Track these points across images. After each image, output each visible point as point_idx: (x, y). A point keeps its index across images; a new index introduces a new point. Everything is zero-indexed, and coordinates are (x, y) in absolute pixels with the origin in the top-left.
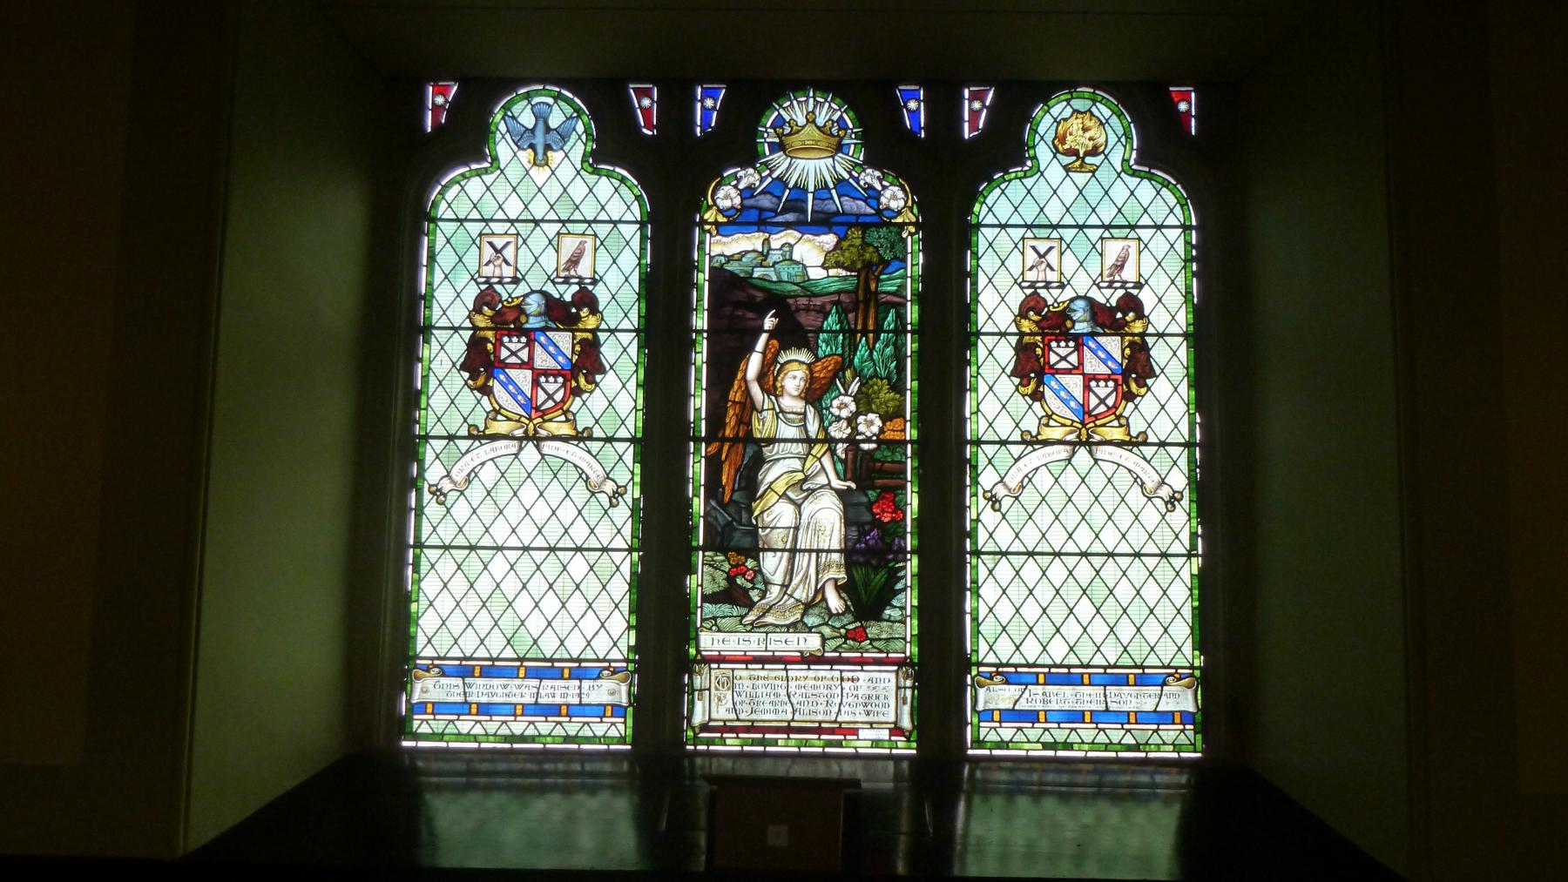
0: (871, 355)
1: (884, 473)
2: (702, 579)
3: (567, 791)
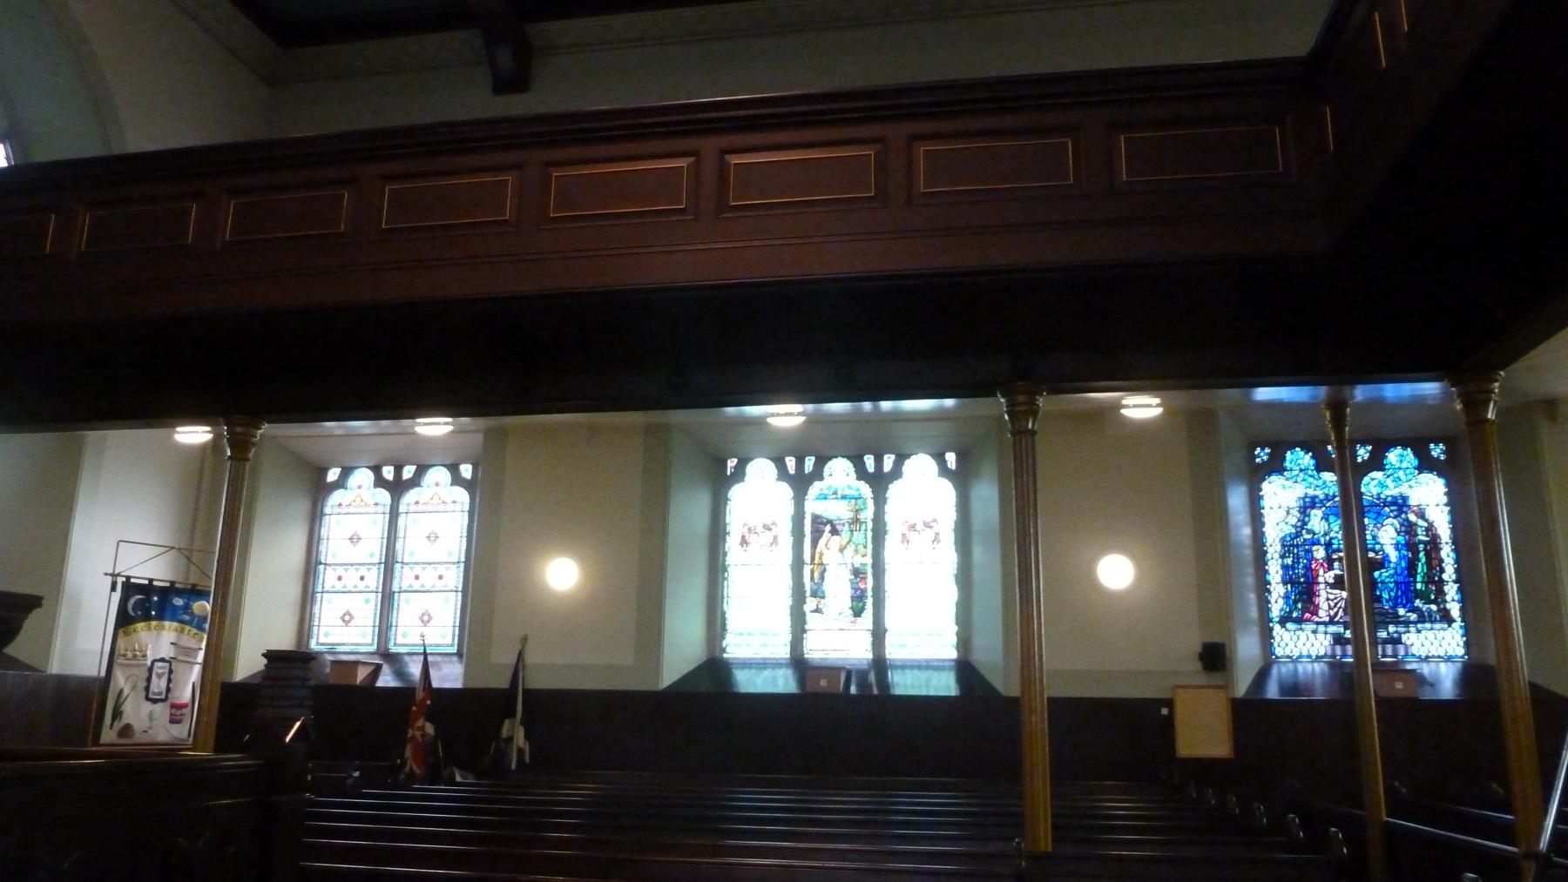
0: (858, 537)
1: (862, 573)
2: (810, 604)
3: (773, 669)
